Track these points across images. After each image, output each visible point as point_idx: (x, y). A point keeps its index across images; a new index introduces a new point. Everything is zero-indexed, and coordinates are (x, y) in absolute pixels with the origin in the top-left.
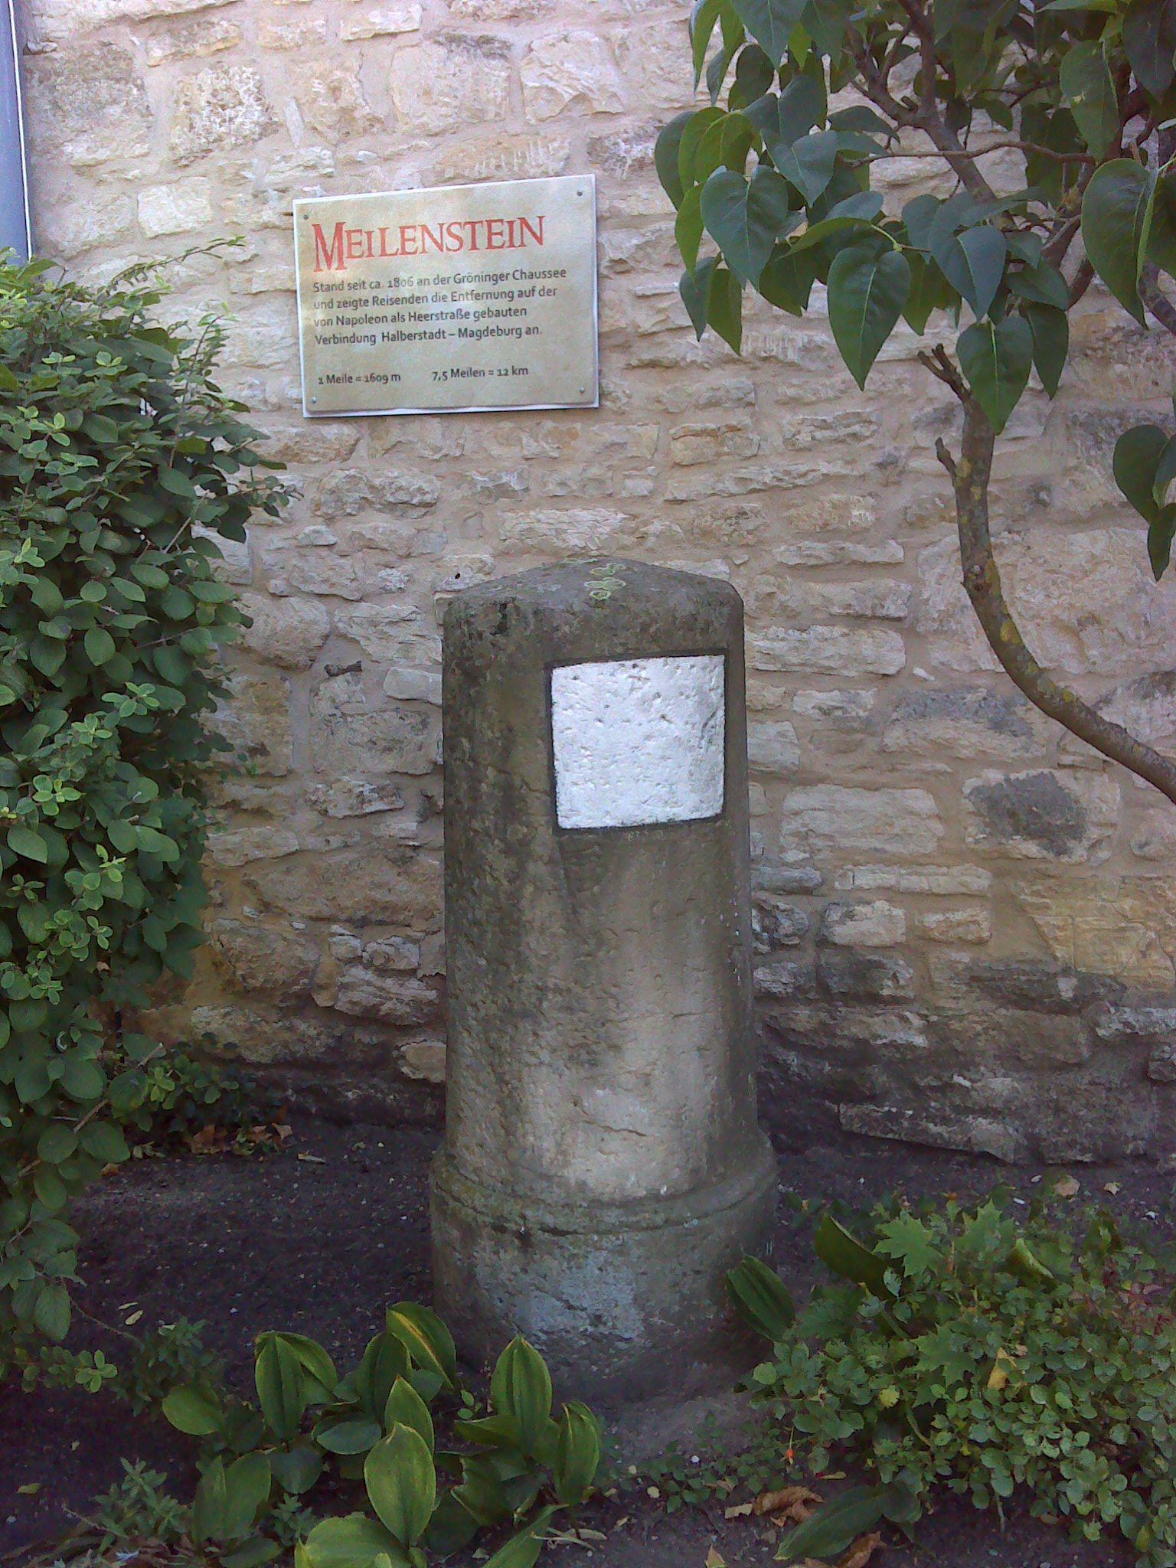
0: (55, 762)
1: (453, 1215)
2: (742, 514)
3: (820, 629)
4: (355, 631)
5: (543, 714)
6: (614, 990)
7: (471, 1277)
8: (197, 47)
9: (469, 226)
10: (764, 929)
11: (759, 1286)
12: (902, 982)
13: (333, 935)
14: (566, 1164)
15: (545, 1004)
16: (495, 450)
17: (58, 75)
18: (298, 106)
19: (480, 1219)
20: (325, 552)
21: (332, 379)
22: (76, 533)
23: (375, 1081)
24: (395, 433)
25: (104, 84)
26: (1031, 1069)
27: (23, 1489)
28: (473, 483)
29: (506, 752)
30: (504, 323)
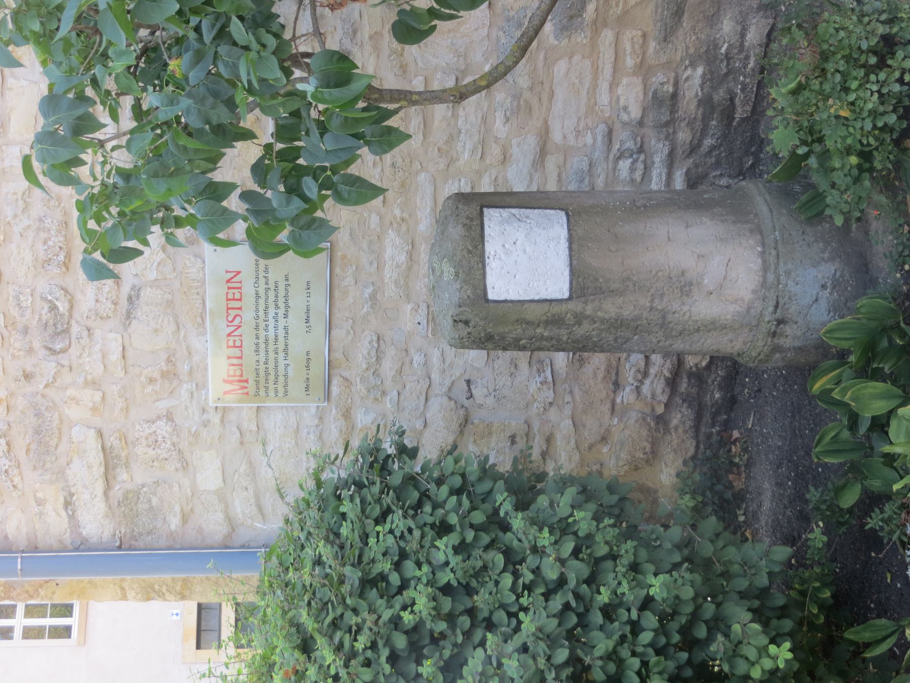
0: (531, 537)
1: (767, 356)
2: (393, 165)
3: (460, 123)
4: (448, 382)
5: (510, 305)
6: (654, 272)
7: (800, 350)
8: (123, 454)
9: (230, 311)
10: (631, 156)
11: (808, 206)
12: (665, 80)
13: (622, 401)
14: (742, 300)
15: (659, 307)
16: (350, 300)
17: (133, 531)
18: (158, 400)
19: (769, 343)
20: (402, 397)
21: (307, 389)
22: (425, 524)
23: (710, 381)
24: (338, 355)
25: (140, 506)
26: (719, 8)
27: (889, 581)
28: (367, 313)
29: (527, 323)
30: (282, 293)
